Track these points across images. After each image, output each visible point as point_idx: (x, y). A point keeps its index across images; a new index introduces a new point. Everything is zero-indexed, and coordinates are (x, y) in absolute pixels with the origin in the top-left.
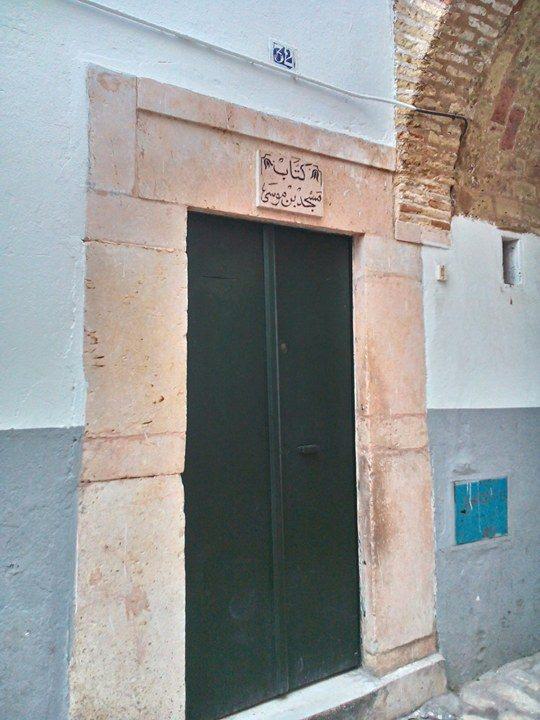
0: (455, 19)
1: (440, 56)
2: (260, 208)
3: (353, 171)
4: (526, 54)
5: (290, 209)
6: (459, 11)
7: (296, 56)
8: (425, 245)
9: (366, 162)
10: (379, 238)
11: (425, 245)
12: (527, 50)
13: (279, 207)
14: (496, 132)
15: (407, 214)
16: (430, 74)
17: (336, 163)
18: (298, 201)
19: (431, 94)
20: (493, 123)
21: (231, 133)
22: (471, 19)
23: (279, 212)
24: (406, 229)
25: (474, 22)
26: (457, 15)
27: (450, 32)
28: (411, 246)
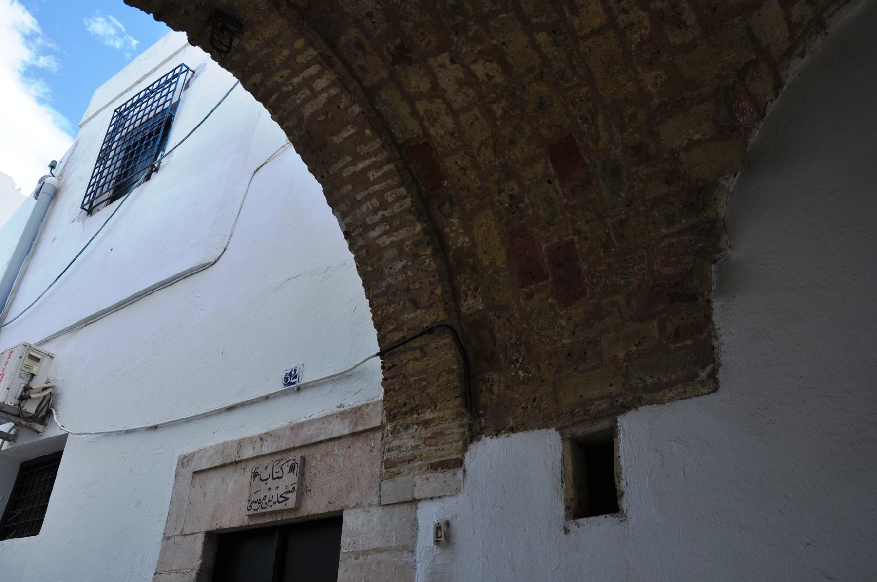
0: (365, 255)
1: (378, 291)
2: (250, 517)
3: (337, 449)
4: (504, 197)
5: (268, 509)
6: (362, 248)
7: (290, 368)
8: (420, 500)
9: (347, 431)
10: (359, 510)
11: (420, 500)
12: (500, 191)
13: (260, 511)
14: (536, 297)
15: (393, 470)
16: (379, 313)
17: (321, 446)
18: (275, 499)
19: (391, 328)
20: (525, 290)
21: (241, 461)
22: (380, 241)
23: (263, 515)
24: (392, 489)
25: (386, 240)
26: (364, 251)
27: (370, 268)
28: (403, 507)
